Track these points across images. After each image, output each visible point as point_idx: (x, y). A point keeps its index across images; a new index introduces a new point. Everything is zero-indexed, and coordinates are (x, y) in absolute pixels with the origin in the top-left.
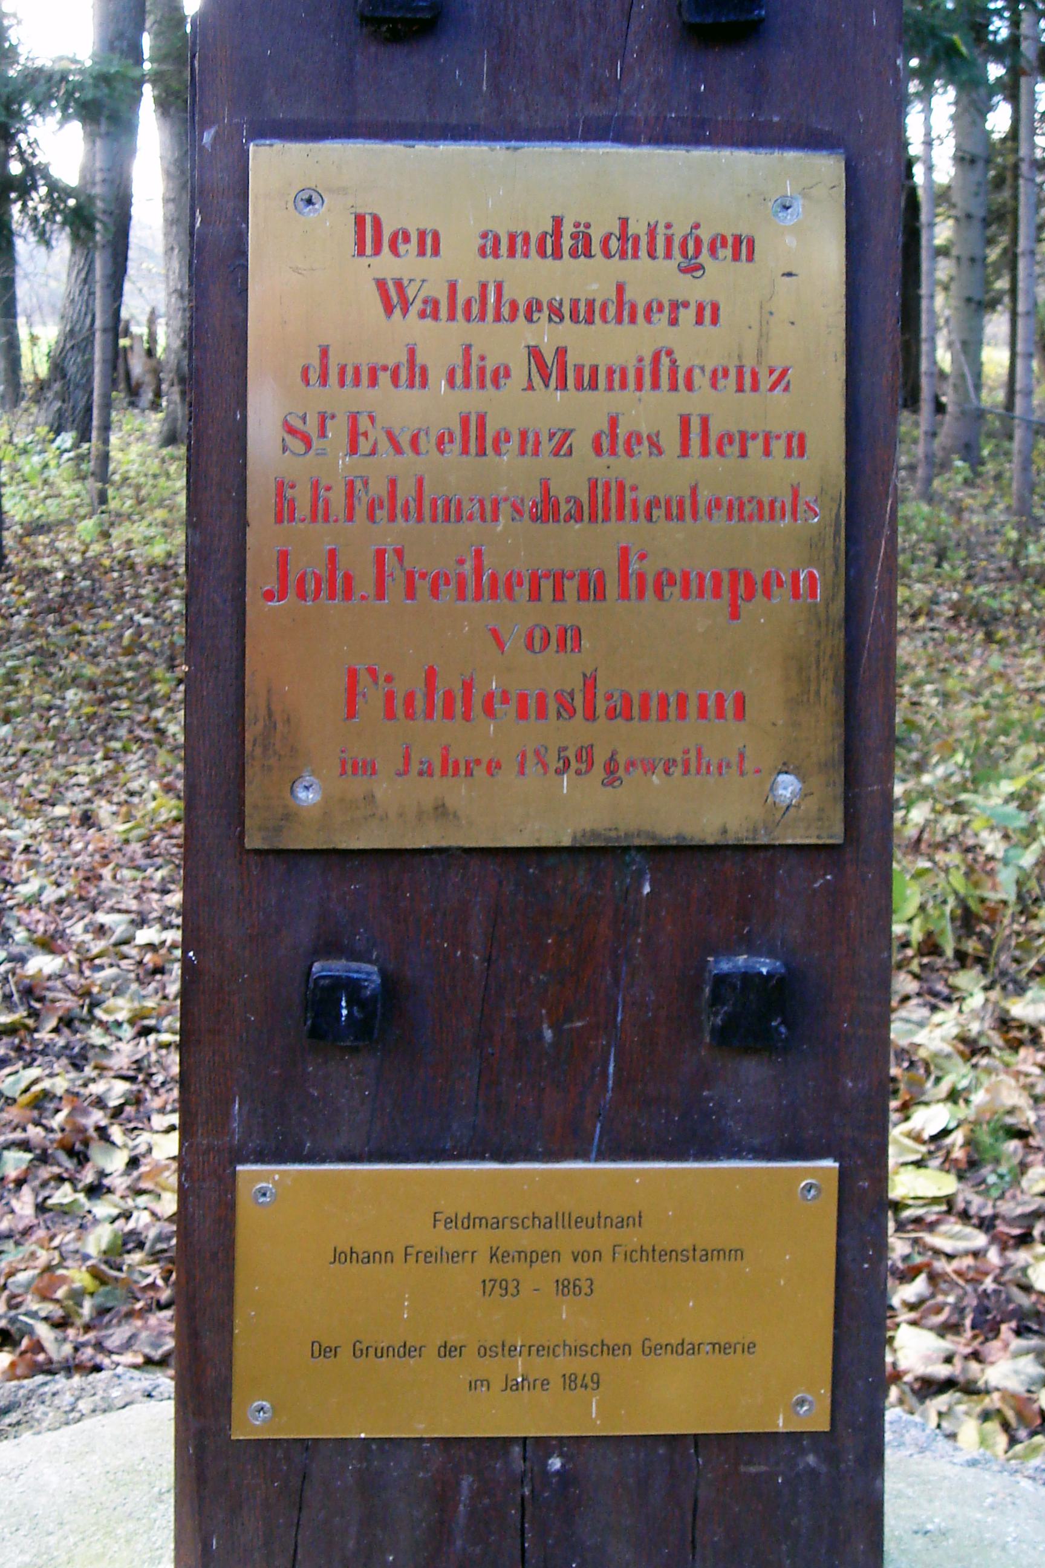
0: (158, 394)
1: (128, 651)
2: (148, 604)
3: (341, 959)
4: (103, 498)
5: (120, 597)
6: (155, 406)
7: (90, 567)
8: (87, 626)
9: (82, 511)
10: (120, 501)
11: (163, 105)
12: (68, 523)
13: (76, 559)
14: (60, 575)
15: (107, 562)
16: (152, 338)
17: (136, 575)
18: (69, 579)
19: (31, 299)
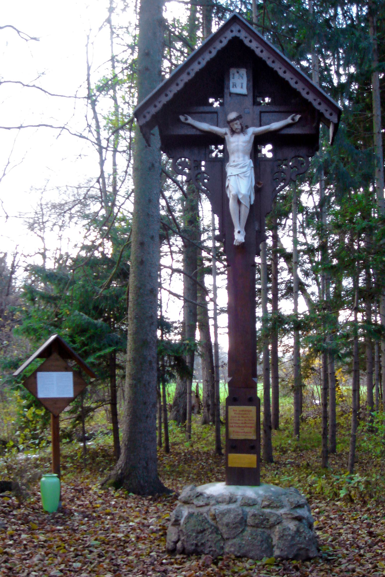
0: (200, 409)
1: (201, 469)
2: (204, 461)
3: (134, 185)
4: (190, 437)
5: (198, 459)
6: (199, 413)
7: (190, 453)
8: (192, 464)
9: (185, 440)
10: (194, 438)
11: (199, 328)
12: (182, 443)
13: (186, 451)
14: (183, 454)
15: (194, 452)
16: (197, 391)
17: (201, 455)
18: (185, 455)
19: (79, 272)
